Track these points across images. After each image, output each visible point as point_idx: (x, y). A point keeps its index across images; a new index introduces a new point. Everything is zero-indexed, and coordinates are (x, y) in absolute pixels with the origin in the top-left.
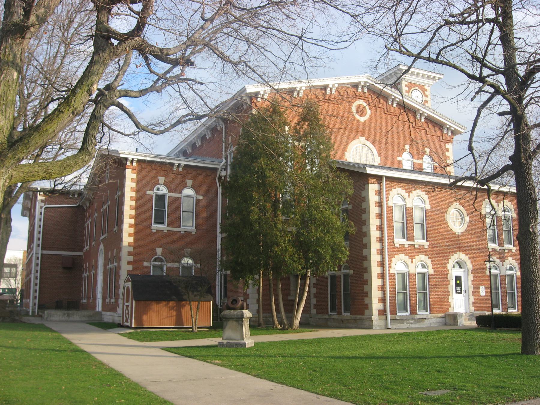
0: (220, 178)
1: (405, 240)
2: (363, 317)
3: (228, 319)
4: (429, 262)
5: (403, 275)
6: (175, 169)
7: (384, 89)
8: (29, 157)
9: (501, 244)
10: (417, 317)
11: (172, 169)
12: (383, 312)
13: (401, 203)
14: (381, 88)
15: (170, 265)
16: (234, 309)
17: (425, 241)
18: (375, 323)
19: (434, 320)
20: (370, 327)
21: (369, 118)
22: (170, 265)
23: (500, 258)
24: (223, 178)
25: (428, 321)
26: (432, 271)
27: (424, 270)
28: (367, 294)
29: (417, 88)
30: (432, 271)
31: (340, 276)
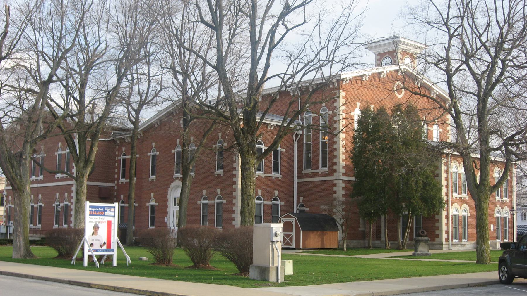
0: (297, 135)
1: (466, 195)
2: (434, 242)
3: (420, 241)
4: (468, 208)
5: (455, 216)
6: (269, 128)
7: (432, 86)
8: (404, 170)
9: (502, 197)
10: (463, 243)
11: (267, 128)
12: (447, 240)
13: (456, 171)
14: (431, 85)
15: (266, 203)
16: (423, 236)
17: (466, 195)
18: (444, 246)
19: (470, 245)
20: (441, 249)
21: (404, 95)
22: (266, 203)
23: (500, 206)
24: (299, 136)
25: (467, 246)
26: (469, 215)
27: (465, 214)
28: (439, 228)
29: (408, 56)
30: (469, 215)
31: (215, 204)
